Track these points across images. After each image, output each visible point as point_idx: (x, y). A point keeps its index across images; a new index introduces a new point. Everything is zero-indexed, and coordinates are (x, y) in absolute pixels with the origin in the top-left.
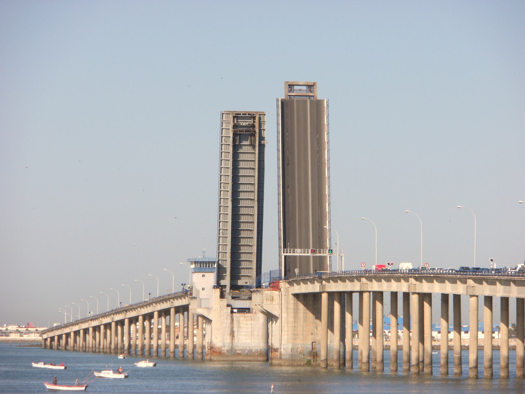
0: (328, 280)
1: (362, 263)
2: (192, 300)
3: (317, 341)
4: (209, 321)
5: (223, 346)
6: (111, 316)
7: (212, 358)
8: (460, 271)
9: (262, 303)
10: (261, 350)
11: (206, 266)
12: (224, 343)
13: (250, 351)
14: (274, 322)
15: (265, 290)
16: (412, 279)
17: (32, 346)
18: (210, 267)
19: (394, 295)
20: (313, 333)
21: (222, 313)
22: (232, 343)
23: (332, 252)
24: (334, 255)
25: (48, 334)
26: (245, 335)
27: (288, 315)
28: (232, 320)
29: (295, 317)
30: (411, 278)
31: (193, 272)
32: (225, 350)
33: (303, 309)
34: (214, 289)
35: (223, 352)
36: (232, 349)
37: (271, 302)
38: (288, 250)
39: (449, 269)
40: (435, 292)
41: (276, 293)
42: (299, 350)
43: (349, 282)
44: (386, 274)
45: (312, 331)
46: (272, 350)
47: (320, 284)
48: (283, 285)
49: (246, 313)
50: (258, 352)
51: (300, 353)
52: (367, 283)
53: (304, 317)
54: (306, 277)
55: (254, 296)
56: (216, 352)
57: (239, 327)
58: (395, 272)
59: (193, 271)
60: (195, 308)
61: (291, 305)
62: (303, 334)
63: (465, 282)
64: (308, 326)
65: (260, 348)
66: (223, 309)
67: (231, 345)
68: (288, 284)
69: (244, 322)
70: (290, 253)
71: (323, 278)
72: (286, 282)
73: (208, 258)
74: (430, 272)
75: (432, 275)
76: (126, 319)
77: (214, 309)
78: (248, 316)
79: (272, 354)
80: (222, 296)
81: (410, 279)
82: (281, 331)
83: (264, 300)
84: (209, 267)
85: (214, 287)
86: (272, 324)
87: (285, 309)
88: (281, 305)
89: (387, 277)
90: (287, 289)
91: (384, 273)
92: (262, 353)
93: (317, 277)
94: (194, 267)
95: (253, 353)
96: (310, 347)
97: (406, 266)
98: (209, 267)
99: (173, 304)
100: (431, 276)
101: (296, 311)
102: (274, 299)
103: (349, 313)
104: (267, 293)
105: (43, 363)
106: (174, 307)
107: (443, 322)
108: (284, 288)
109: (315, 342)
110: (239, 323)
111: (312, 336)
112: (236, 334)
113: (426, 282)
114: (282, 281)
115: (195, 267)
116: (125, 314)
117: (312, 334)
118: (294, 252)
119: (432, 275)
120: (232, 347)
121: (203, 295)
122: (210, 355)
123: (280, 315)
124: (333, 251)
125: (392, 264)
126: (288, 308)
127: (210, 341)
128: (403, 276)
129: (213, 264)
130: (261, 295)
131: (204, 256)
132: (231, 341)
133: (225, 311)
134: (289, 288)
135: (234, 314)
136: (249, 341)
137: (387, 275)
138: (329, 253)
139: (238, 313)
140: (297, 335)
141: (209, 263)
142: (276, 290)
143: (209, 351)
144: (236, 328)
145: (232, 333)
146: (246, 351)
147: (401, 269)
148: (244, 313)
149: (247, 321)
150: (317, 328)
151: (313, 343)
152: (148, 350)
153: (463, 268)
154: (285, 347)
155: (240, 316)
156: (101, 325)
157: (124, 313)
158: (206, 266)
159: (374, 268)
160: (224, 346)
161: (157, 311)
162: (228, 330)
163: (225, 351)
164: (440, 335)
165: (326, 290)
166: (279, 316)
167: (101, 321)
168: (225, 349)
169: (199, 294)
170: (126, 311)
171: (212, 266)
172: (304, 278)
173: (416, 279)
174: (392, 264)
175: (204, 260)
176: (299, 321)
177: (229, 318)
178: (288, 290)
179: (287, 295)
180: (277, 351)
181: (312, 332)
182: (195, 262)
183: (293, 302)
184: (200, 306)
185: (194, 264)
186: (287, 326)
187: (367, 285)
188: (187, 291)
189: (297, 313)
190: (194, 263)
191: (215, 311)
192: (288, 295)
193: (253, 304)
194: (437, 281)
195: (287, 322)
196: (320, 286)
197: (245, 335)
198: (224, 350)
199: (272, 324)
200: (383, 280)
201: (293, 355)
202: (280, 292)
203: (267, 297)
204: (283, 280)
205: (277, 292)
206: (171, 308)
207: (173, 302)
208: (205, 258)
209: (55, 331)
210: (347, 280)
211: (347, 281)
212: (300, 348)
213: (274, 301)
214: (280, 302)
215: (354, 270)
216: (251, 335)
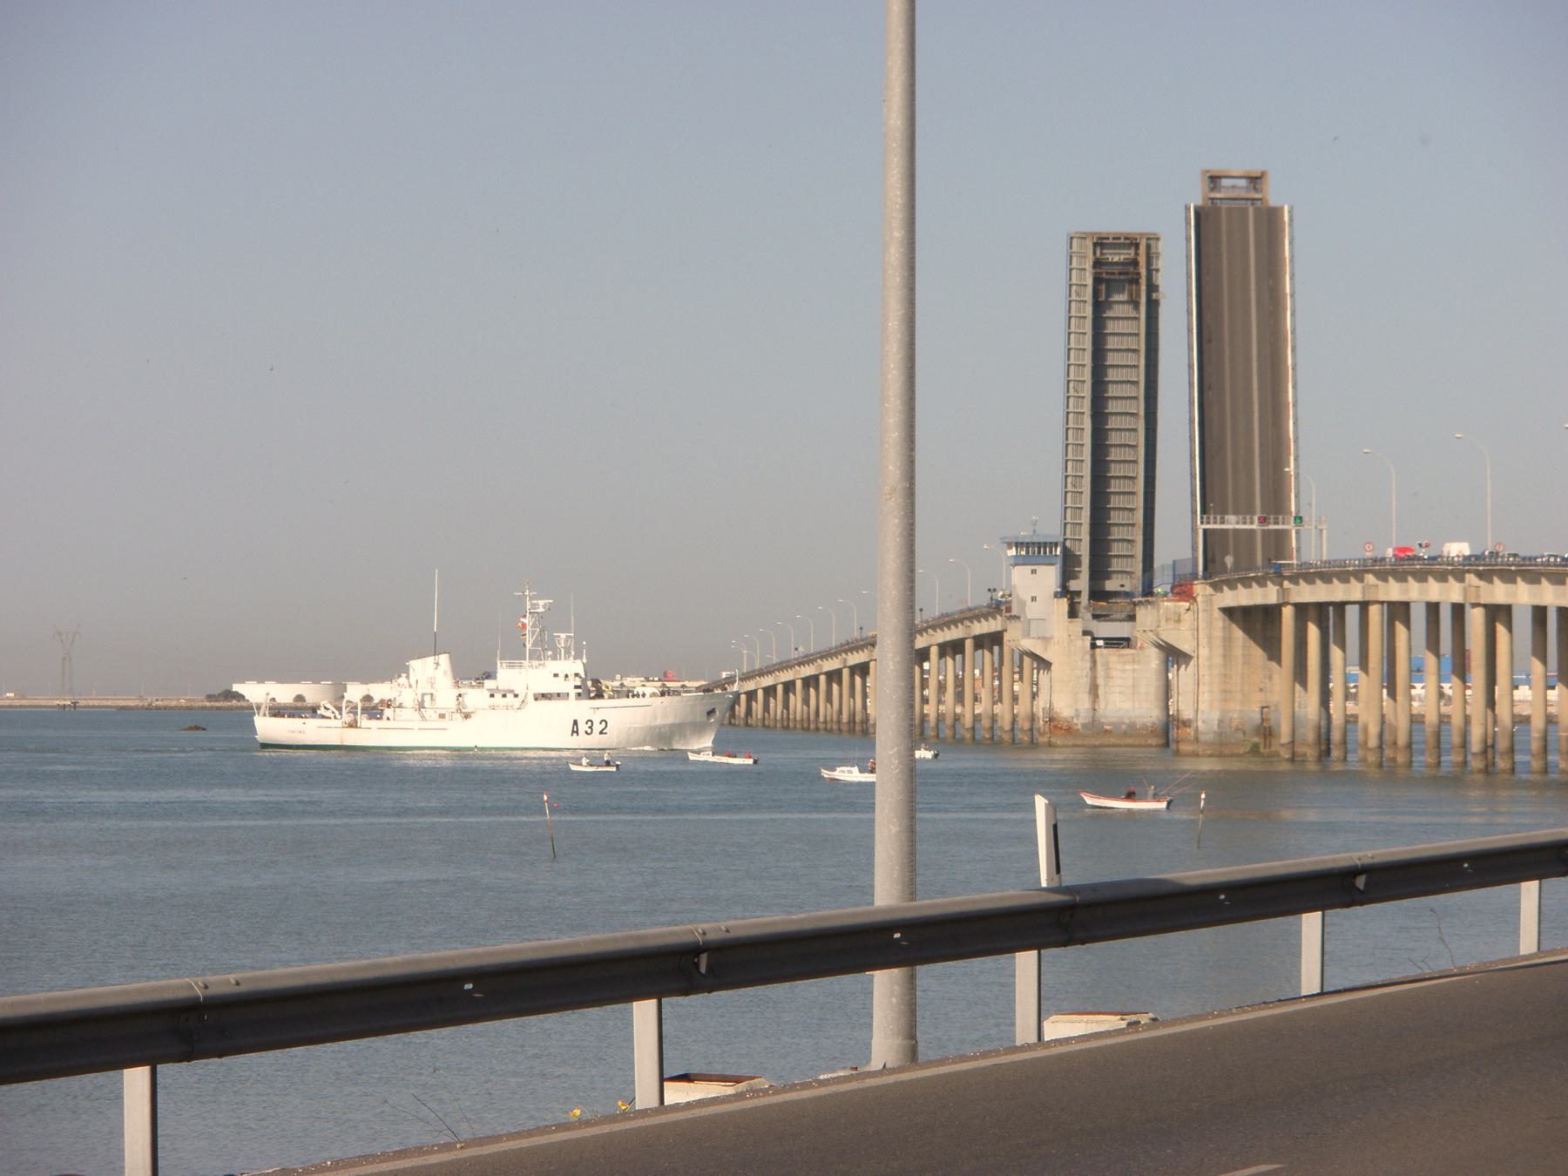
0: (1294, 579)
3: (1270, 705)
4: (1044, 664)
7: (1051, 739)
9: (1159, 626)
10: (1154, 724)
12: (1077, 710)
13: (1132, 726)
14: (1184, 666)
19: (1433, 609)
21: (1072, 648)
23: (1301, 521)
24: (1306, 527)
28: (1094, 662)
29: (1225, 656)
37: (1177, 625)
42: (1235, 723)
48: (1201, 589)
49: (1123, 648)
50: (1147, 727)
51: (1237, 729)
53: (1244, 655)
56: (1061, 728)
57: (1108, 677)
59: (1012, 562)
60: (1016, 638)
67: (1091, 714)
70: (1215, 523)
75: (1513, 568)
77: (1056, 640)
78: (1127, 655)
80: (1073, 613)
81: (1467, 576)
91: (1413, 565)
96: (1257, 716)
97: (1457, 549)
100: (1511, 570)
106: (972, 635)
109: (1268, 707)
112: (1101, 691)
119: (1513, 568)
121: (1032, 611)
127: (1048, 706)
133: (1079, 643)
135: (1098, 650)
136: (1127, 705)
139: (1105, 648)
143: (1047, 726)
145: (1094, 689)
146: (1124, 727)
149: (1125, 663)
150: (1270, 678)
151: (1263, 708)
157: (867, 648)
159: (1390, 553)
160: (1077, 716)
163: (1079, 727)
166: (1192, 654)
168: (1079, 723)
171: (1051, 552)
173: (1480, 575)
177: (1088, 657)
178: (1211, 600)
180: (1190, 726)
184: (1027, 634)
185: (1014, 549)
186: (1210, 675)
194: (1524, 580)
195: (1210, 667)
198: (1077, 724)
208: (1038, 535)
213: (1182, 623)
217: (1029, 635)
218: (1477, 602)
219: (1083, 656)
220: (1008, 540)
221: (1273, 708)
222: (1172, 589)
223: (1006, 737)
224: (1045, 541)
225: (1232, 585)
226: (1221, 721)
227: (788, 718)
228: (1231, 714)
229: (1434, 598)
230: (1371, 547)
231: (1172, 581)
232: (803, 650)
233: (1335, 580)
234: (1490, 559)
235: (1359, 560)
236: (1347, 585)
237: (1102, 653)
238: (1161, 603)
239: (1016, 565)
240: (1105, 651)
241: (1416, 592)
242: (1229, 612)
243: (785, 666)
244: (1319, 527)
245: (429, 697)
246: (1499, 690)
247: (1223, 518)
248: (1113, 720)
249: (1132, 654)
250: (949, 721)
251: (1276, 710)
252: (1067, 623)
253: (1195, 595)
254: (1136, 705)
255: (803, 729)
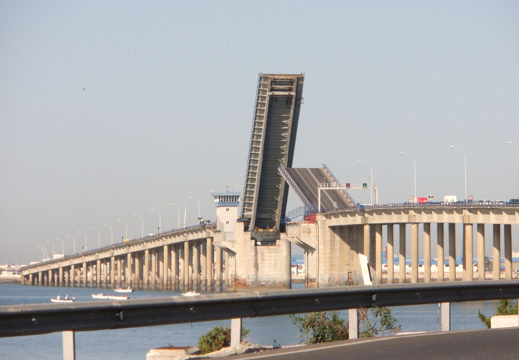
0: (371, 213)
1: (410, 197)
2: (219, 234)
3: (352, 271)
4: (232, 253)
5: (248, 278)
6: (110, 251)
7: (236, 289)
8: (510, 203)
9: (300, 235)
10: (285, 281)
11: (230, 200)
12: (248, 275)
13: (274, 282)
14: (311, 254)
15: (302, 223)
16: (467, 210)
17: (5, 283)
18: (233, 201)
19: (440, 226)
20: (349, 264)
21: (246, 246)
22: (256, 274)
23: (366, 186)
24: (368, 188)
25: (29, 270)
26: (268, 267)
27: (325, 246)
28: (256, 252)
29: (331, 249)
30: (465, 210)
31: (217, 207)
32: (250, 282)
33: (339, 241)
34: (238, 223)
35: (248, 284)
36: (256, 281)
37: (308, 234)
38: (324, 184)
39: (498, 201)
40: (491, 223)
41: (312, 226)
42: (336, 280)
43: (394, 214)
44: (437, 206)
45: (348, 262)
46: (308, 280)
47: (362, 217)
48: (320, 218)
49: (270, 245)
50: (281, 283)
51: (337, 283)
52: (415, 215)
53: (340, 248)
54: (346, 210)
55: (290, 228)
56: (241, 284)
57: (263, 259)
58: (432, 205)
59: (217, 205)
60: (220, 241)
61: (328, 237)
62: (339, 264)
63: (407, 213)
64: (344, 256)
65: (284, 279)
66: (247, 242)
67: (255, 277)
68: (324, 217)
69: (268, 255)
70: (326, 187)
71: (366, 210)
72: (322, 215)
73: (232, 193)
74: (496, 204)
75: (488, 207)
76: (128, 253)
77: (238, 242)
78: (272, 249)
79: (309, 284)
80: (246, 229)
81: (464, 211)
82: (318, 262)
83: (302, 233)
84: (233, 201)
85: (239, 220)
86: (308, 255)
87: (322, 241)
88: (317, 237)
89: (438, 209)
90: (323, 222)
91: (515, 206)
92: (285, 285)
93: (359, 210)
94: (219, 201)
95: (276, 284)
96: (347, 277)
97: (450, 199)
98: (233, 201)
99: (187, 238)
100: (488, 208)
101: (332, 243)
102: (311, 231)
103: (390, 243)
104: (304, 225)
105: (102, 294)
106: (188, 240)
107: (496, 250)
108: (321, 221)
109: (351, 272)
110: (263, 255)
111: (348, 266)
112: (260, 266)
113: (481, 214)
114: (319, 214)
115: (220, 201)
116: (128, 248)
117: (348, 265)
118: (329, 187)
119: (488, 207)
120: (256, 279)
121: (227, 228)
122: (234, 287)
123: (317, 247)
124: (367, 185)
125: (432, 197)
126: (324, 240)
127: (234, 273)
128: (456, 208)
129: (237, 199)
130: (299, 228)
131: (228, 190)
132: (255, 273)
133: (249, 243)
134: (325, 220)
135: (258, 247)
136: (272, 273)
137: (438, 207)
138: (363, 186)
139: (261, 246)
140: (334, 265)
141: (233, 197)
142: (313, 222)
143: (233, 283)
144: (260, 260)
145: (256, 266)
146: (270, 283)
147: (446, 202)
148: (268, 245)
149: (270, 253)
150: (352, 259)
151: (349, 273)
152: (154, 284)
153: (513, 200)
154: (322, 277)
155: (264, 249)
156: (98, 260)
157: (126, 247)
158: (230, 200)
159: (416, 201)
160: (249, 278)
161: (167, 245)
162: (252, 262)
163: (250, 283)
164: (411, 268)
165: (368, 222)
166: (316, 248)
167: (98, 256)
168: (249, 281)
169: (223, 227)
170: (129, 246)
171: (236, 200)
172: (344, 210)
173: (470, 211)
174: (432, 197)
175: (228, 195)
176: (335, 252)
177: (253, 250)
178: (325, 223)
179: (324, 228)
180: (314, 282)
181: (348, 262)
182: (219, 197)
183: (329, 234)
184: (224, 239)
185: (218, 199)
186: (324, 257)
187: (415, 217)
188: (204, 225)
189: (333, 244)
190: (218, 197)
191: (239, 244)
192: (325, 227)
193: (289, 236)
194: (493, 212)
195: (325, 254)
196: (362, 218)
197: (268, 267)
198: (249, 282)
199: (308, 255)
200: (433, 212)
201: (330, 284)
202: (317, 224)
203: (304, 230)
204: (319, 213)
205: (313, 225)
206: (185, 242)
207: (187, 236)
208: (229, 193)
209: (39, 267)
210: (392, 212)
211: (393, 213)
212: (336, 277)
213: (311, 233)
214: (316, 234)
215: (389, 203)
216: (275, 267)
217: (225, 240)
218: (469, 223)
219: (251, 250)
220: (215, 195)
221: (353, 273)
222: (304, 218)
223: (153, 287)
224: (228, 195)
225: (336, 216)
226: (329, 279)
227: (171, 284)
228: (334, 276)
229: (481, 221)
230: (412, 198)
231: (304, 214)
232: (87, 248)
233: (393, 213)
234: (468, 203)
235: (392, 204)
236: (399, 215)
237: (260, 248)
238: (301, 224)
239: (219, 207)
240: (262, 247)
241: (434, 218)
242: (333, 228)
243: (77, 256)
244: (374, 188)
245: (306, 287)
246: (194, 257)
247: (329, 184)
248: (265, 280)
249: (274, 248)
250: (218, 283)
251: (355, 274)
252: (244, 234)
253: (317, 221)
254: (276, 272)
255: (52, 285)
